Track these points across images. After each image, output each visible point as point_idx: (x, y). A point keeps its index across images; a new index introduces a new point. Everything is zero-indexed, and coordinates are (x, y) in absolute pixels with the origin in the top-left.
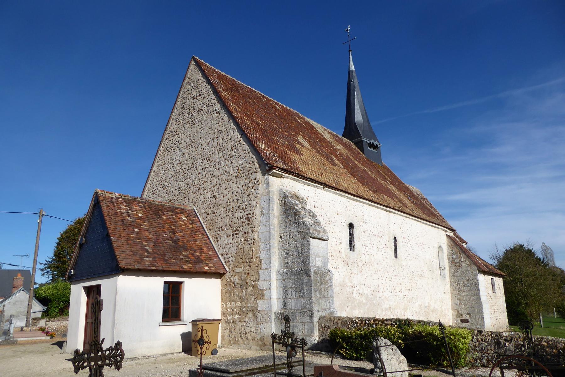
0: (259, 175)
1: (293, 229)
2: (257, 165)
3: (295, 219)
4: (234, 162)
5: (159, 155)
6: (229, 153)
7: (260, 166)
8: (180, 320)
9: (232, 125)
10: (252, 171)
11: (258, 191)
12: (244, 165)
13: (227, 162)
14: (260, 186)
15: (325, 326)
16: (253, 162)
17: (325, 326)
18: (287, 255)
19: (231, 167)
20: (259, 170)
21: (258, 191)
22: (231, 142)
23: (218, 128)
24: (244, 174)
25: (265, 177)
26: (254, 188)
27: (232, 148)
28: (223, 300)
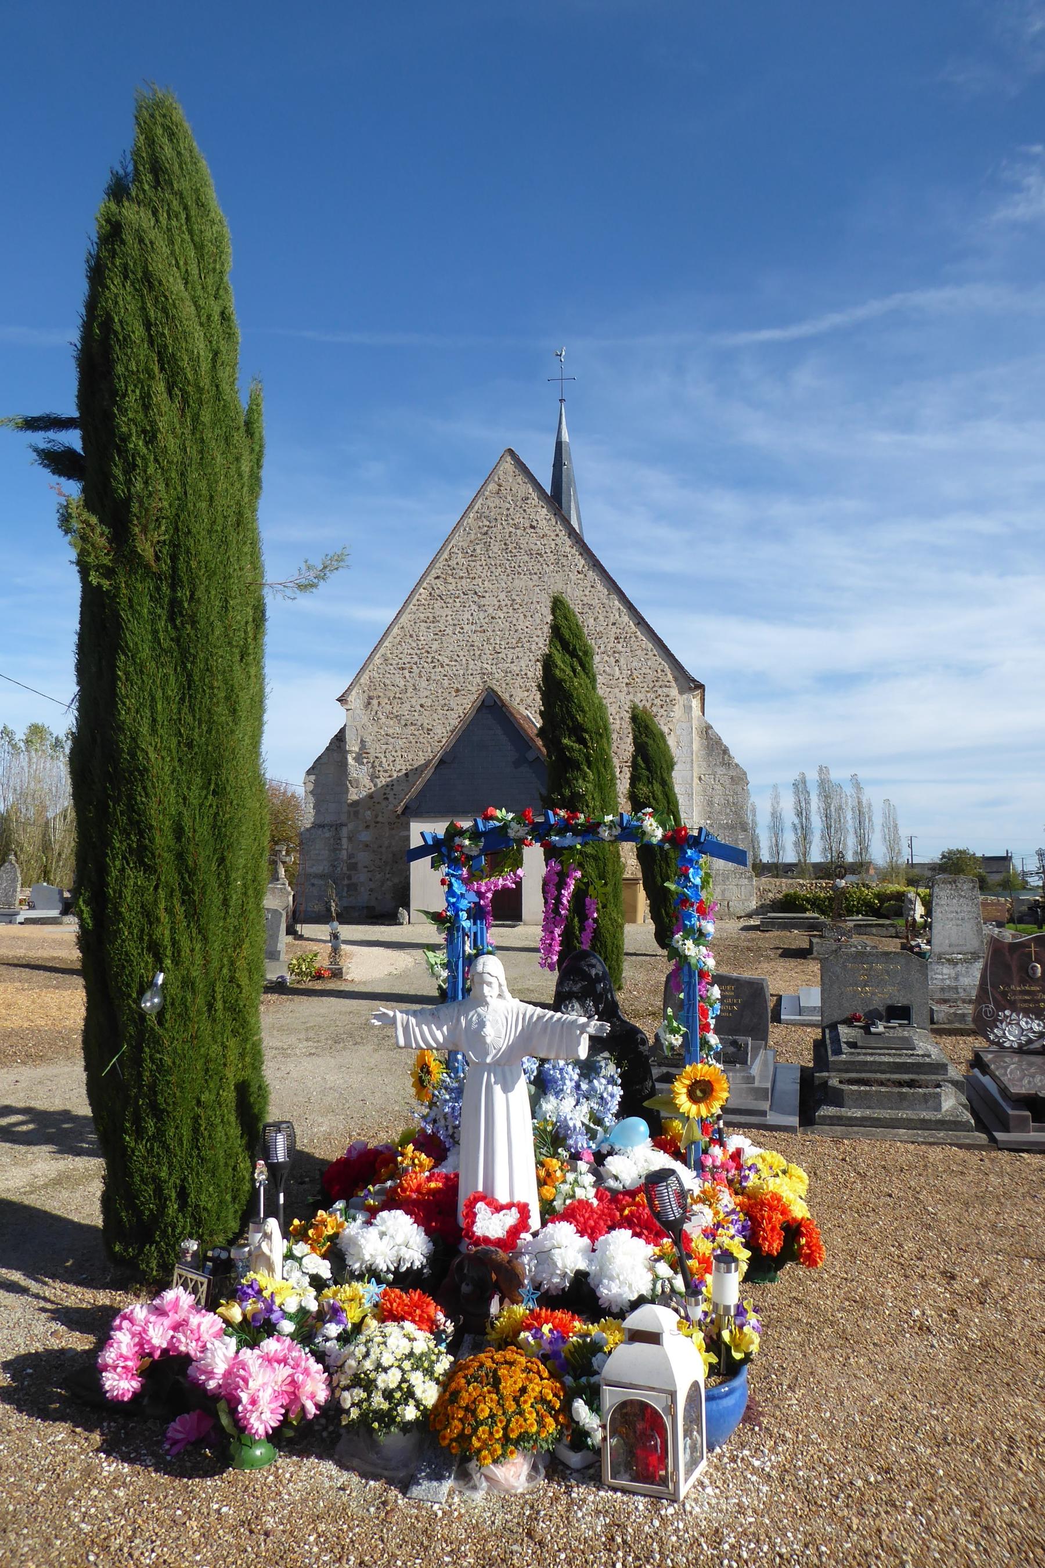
0: (674, 692)
1: (720, 771)
2: (670, 677)
3: (723, 758)
4: (622, 661)
5: (414, 601)
6: (612, 645)
7: (676, 679)
8: (521, 920)
9: (617, 602)
10: (660, 683)
11: (672, 714)
12: (644, 671)
13: (606, 658)
14: (677, 706)
15: (764, 890)
16: (663, 671)
17: (764, 890)
18: (710, 803)
19: (617, 668)
20: (673, 684)
21: (672, 714)
22: (614, 629)
23: (583, 598)
24: (645, 685)
25: (685, 696)
26: (665, 708)
27: (616, 638)
28: (409, 836)
